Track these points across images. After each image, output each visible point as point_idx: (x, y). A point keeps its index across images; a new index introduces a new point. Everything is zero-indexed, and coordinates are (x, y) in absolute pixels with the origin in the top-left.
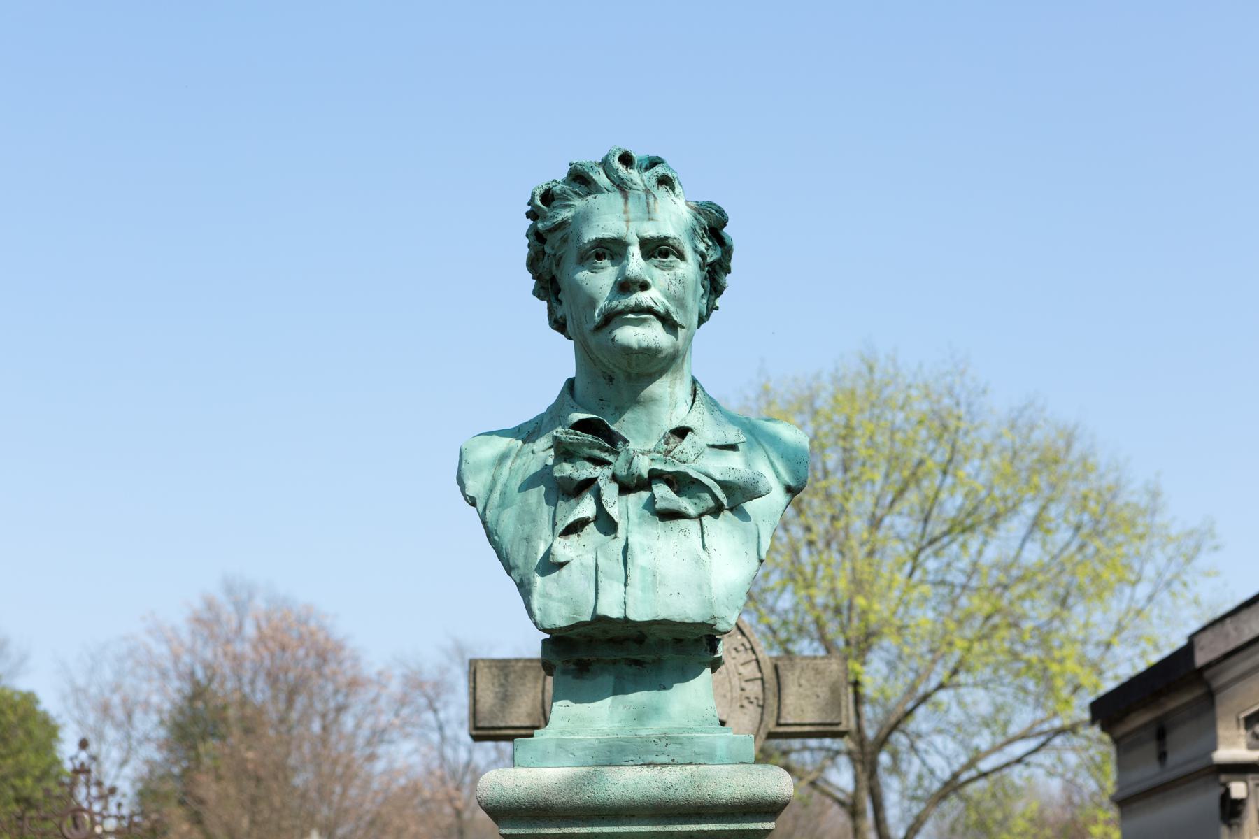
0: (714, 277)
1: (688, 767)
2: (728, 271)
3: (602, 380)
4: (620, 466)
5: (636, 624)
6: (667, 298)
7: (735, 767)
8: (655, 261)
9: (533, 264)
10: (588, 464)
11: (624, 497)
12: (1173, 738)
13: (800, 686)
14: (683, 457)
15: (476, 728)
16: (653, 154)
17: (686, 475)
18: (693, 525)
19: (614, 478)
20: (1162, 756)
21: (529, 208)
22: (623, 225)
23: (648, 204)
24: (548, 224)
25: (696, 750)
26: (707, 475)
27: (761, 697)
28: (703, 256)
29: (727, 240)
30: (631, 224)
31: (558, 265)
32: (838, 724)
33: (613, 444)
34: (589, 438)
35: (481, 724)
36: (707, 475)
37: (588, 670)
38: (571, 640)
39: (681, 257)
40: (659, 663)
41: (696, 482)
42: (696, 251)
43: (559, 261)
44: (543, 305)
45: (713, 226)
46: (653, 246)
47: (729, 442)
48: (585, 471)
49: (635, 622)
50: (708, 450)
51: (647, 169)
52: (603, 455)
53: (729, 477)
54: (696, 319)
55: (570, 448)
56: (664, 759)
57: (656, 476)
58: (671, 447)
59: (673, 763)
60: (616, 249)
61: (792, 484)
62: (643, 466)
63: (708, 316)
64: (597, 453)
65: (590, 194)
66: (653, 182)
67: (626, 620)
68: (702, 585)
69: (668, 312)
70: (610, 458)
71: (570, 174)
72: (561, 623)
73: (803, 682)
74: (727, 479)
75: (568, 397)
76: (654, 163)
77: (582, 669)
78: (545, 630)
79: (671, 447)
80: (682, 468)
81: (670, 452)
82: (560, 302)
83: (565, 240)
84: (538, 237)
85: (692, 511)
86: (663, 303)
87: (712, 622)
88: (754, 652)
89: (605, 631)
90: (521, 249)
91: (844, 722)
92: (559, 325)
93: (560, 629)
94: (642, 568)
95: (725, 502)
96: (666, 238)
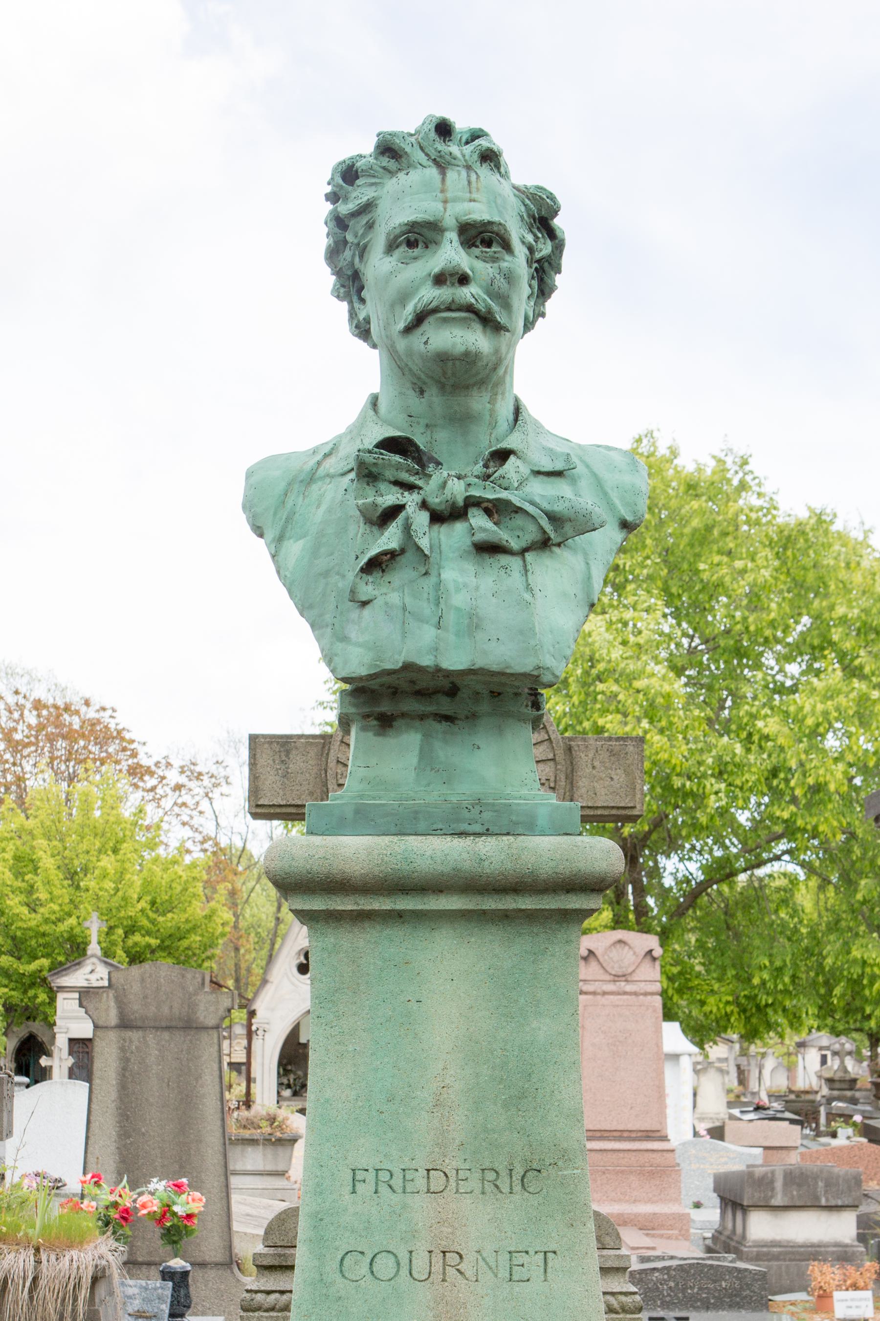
0: (544, 272)
1: (505, 838)
2: (559, 271)
3: (411, 393)
4: (431, 489)
5: (448, 674)
6: (489, 295)
7: (559, 838)
8: (476, 251)
9: (333, 254)
10: (395, 489)
11: (436, 527)
13: (594, 768)
14: (505, 483)
15: (258, 806)
16: (476, 125)
17: (507, 503)
18: (515, 563)
19: (424, 505)
21: (329, 189)
22: (440, 206)
23: (469, 182)
25: (514, 818)
26: (532, 503)
27: (552, 779)
28: (531, 249)
29: (558, 233)
30: (449, 205)
31: (361, 257)
32: (633, 808)
33: (423, 466)
34: (397, 458)
36: (532, 503)
37: (391, 726)
38: (373, 691)
39: (507, 246)
40: (473, 717)
41: (518, 510)
42: (523, 243)
43: (363, 251)
44: (344, 306)
45: (542, 217)
46: (473, 232)
47: (556, 469)
48: (390, 497)
49: (446, 671)
50: (532, 478)
51: (467, 143)
52: (412, 479)
53: (558, 508)
54: (521, 323)
55: (374, 470)
56: (477, 828)
57: (472, 502)
58: (491, 470)
59: (488, 833)
60: (429, 234)
61: (629, 518)
62: (457, 490)
63: (533, 323)
64: (405, 477)
66: (476, 157)
67: (438, 670)
68: (526, 632)
69: (490, 311)
70: (419, 483)
71: (378, 147)
72: (364, 672)
73: (597, 764)
75: (372, 413)
76: (476, 135)
77: (385, 723)
78: (345, 680)
79: (491, 470)
80: (504, 495)
81: (489, 476)
82: (362, 301)
83: (370, 226)
84: (340, 223)
85: (515, 545)
86: (484, 300)
87: (535, 673)
88: (547, 732)
89: (413, 682)
90: (320, 239)
91: (638, 806)
92: (363, 331)
93: (361, 679)
94: (458, 609)
95: (552, 535)
96: (490, 223)
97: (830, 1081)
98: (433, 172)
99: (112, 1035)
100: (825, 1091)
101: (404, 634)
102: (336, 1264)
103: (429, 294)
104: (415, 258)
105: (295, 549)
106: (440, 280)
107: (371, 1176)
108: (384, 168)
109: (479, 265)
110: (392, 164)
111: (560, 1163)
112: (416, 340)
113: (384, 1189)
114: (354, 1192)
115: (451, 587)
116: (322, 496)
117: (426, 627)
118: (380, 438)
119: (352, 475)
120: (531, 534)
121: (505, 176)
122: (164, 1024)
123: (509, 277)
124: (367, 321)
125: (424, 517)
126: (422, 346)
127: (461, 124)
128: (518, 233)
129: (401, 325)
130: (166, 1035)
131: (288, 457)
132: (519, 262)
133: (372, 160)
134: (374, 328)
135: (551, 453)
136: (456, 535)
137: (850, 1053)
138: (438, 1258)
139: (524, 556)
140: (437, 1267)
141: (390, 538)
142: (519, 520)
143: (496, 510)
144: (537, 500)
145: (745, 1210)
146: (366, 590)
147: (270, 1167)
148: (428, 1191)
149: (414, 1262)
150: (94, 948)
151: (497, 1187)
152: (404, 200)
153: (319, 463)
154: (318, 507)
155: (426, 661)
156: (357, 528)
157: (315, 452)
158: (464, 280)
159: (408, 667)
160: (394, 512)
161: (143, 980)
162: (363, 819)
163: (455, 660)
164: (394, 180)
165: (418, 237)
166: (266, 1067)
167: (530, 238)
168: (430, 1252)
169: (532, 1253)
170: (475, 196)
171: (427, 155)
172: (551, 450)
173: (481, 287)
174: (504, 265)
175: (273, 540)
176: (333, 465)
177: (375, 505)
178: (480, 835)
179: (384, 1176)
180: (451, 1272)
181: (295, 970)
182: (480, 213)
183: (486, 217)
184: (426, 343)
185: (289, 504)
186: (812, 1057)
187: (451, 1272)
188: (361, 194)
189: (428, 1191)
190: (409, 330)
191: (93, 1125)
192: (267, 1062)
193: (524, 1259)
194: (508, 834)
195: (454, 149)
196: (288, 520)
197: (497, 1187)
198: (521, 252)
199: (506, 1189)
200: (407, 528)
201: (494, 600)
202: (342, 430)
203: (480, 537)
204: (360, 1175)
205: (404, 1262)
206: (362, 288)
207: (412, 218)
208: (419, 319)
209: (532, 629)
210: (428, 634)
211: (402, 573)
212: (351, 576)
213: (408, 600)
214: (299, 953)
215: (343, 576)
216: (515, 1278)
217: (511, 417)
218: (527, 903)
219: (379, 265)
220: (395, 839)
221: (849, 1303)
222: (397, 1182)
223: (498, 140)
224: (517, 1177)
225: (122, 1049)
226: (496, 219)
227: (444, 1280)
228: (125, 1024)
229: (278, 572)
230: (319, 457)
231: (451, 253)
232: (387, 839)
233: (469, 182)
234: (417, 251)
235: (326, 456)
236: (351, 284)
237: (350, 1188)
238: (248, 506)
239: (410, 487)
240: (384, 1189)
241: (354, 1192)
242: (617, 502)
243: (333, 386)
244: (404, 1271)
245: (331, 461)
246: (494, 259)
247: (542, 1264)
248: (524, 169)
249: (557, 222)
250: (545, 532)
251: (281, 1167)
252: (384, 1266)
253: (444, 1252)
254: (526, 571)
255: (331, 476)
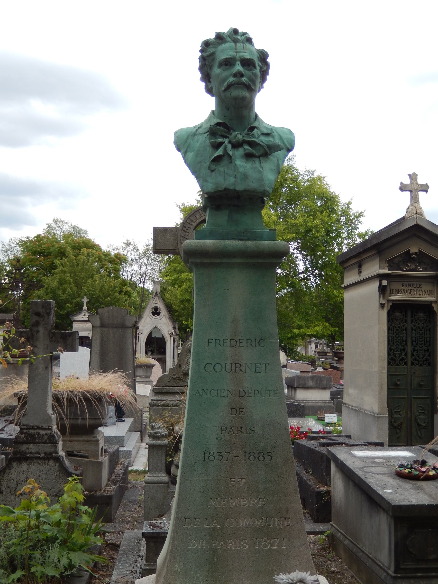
5: (238, 192)
8: (246, 67)
12: (363, 267)
15: (156, 249)
17: (255, 142)
18: (257, 160)
20: (360, 273)
23: (244, 47)
24: (207, 53)
26: (262, 142)
35: (157, 248)
39: (255, 67)
43: (211, 67)
48: (220, 140)
53: (270, 143)
56: (246, 238)
59: (249, 240)
64: (224, 134)
65: (223, 43)
66: (245, 40)
67: (235, 190)
68: (261, 180)
70: (229, 136)
72: (212, 191)
74: (269, 144)
78: (206, 193)
80: (254, 139)
82: (210, 82)
85: (257, 154)
93: (212, 193)
94: (241, 173)
96: (250, 59)
97: (318, 353)
98: (232, 44)
99: (98, 329)
100: (317, 356)
101: (225, 179)
102: (203, 367)
103: (231, 79)
104: (227, 69)
105: (190, 155)
106: (235, 75)
107: (213, 341)
108: (218, 43)
109: (247, 72)
110: (220, 41)
111: (270, 338)
112: (228, 94)
113: (217, 345)
114: (209, 346)
115: (239, 166)
116: (198, 140)
117: (231, 178)
118: (216, 122)
119: (208, 133)
120: (261, 151)
121: (253, 46)
122: (115, 326)
123: (255, 75)
124: (212, 88)
125: (230, 146)
126: (229, 95)
127: (241, 30)
128: (257, 62)
129: (223, 89)
130: (116, 330)
131: (187, 128)
132: (257, 71)
133: (214, 40)
134: (214, 90)
135: (267, 128)
136: (240, 152)
137: (325, 344)
138: (234, 366)
139: (260, 159)
140: (234, 368)
141: (220, 152)
142: (258, 147)
143: (252, 144)
144: (264, 141)
145: (295, 389)
146: (213, 167)
147: (145, 375)
148: (231, 346)
149: (227, 366)
150: (85, 307)
151: (251, 344)
152: (225, 51)
153: (197, 130)
154: (198, 142)
155: (232, 188)
156: (209, 149)
157: (195, 127)
158: (242, 75)
159: (226, 189)
160: (221, 144)
161: (108, 312)
162: (210, 235)
163: (240, 188)
164: (221, 46)
165: (228, 63)
166: (142, 345)
167: (260, 64)
168: (231, 364)
169: (262, 364)
170: (245, 51)
171: (231, 39)
172: (266, 127)
173: (247, 78)
174: (254, 72)
175: (183, 153)
176: (201, 131)
177: (215, 142)
178: (247, 240)
179: (218, 341)
180: (238, 370)
181: (151, 314)
182: (247, 56)
183: (249, 57)
184: (231, 94)
185: (188, 142)
186: (313, 345)
187: (238, 370)
188: (211, 50)
189: (231, 346)
190: (225, 90)
191: (92, 358)
192: (142, 343)
193: (260, 366)
194: (255, 240)
195: (239, 37)
196: (188, 147)
197: (251, 344)
198: (258, 68)
199: (254, 345)
200: (225, 149)
201: (251, 170)
202: (203, 121)
203: (247, 151)
204: (210, 341)
205: (224, 366)
206: (210, 78)
207: (227, 57)
208: (229, 87)
209: (263, 179)
210: (232, 180)
211: (225, 161)
212: (208, 163)
213: (226, 170)
214: (152, 309)
215: (206, 163)
216: (257, 371)
217: (254, 118)
218: (261, 261)
219: (216, 70)
220: (222, 241)
221: (329, 418)
222: (221, 343)
223: (251, 35)
224: (257, 342)
225: (102, 334)
226: (252, 58)
227: (236, 372)
228: (102, 326)
229: (185, 162)
230: (197, 128)
231: (238, 67)
232: (219, 241)
233: (244, 47)
234: (227, 67)
235: (199, 128)
236: (206, 77)
237: (207, 345)
238: (175, 143)
239: (226, 137)
240: (217, 345)
241: (209, 346)
242: (286, 143)
243: (200, 107)
244: (224, 369)
245: (201, 129)
246: (250, 70)
247: (265, 367)
248: (258, 45)
249: (268, 60)
250: (266, 151)
251: (148, 375)
252: (218, 368)
253: (236, 364)
254: (261, 162)
255: (201, 134)
